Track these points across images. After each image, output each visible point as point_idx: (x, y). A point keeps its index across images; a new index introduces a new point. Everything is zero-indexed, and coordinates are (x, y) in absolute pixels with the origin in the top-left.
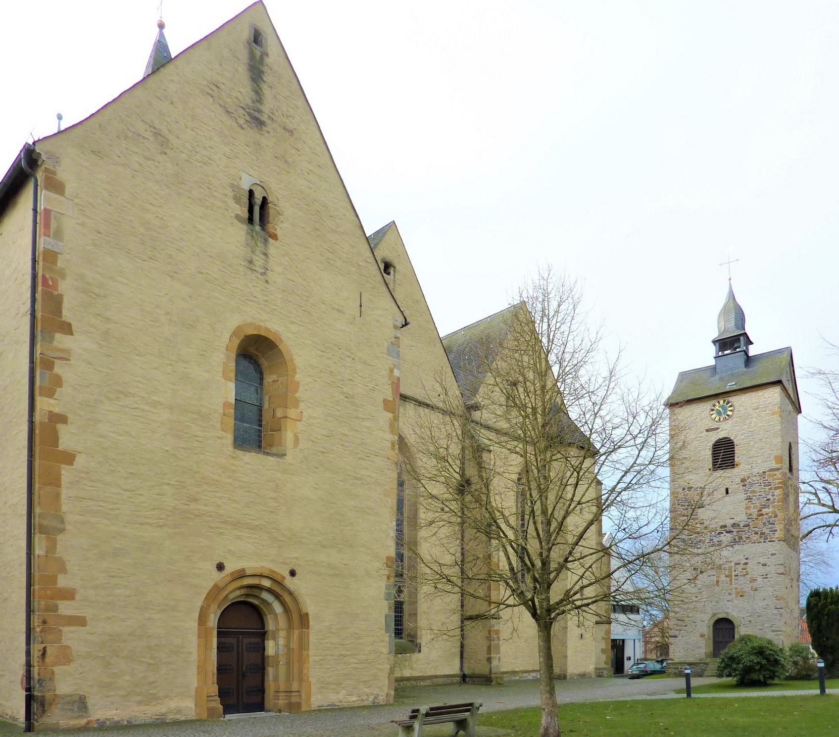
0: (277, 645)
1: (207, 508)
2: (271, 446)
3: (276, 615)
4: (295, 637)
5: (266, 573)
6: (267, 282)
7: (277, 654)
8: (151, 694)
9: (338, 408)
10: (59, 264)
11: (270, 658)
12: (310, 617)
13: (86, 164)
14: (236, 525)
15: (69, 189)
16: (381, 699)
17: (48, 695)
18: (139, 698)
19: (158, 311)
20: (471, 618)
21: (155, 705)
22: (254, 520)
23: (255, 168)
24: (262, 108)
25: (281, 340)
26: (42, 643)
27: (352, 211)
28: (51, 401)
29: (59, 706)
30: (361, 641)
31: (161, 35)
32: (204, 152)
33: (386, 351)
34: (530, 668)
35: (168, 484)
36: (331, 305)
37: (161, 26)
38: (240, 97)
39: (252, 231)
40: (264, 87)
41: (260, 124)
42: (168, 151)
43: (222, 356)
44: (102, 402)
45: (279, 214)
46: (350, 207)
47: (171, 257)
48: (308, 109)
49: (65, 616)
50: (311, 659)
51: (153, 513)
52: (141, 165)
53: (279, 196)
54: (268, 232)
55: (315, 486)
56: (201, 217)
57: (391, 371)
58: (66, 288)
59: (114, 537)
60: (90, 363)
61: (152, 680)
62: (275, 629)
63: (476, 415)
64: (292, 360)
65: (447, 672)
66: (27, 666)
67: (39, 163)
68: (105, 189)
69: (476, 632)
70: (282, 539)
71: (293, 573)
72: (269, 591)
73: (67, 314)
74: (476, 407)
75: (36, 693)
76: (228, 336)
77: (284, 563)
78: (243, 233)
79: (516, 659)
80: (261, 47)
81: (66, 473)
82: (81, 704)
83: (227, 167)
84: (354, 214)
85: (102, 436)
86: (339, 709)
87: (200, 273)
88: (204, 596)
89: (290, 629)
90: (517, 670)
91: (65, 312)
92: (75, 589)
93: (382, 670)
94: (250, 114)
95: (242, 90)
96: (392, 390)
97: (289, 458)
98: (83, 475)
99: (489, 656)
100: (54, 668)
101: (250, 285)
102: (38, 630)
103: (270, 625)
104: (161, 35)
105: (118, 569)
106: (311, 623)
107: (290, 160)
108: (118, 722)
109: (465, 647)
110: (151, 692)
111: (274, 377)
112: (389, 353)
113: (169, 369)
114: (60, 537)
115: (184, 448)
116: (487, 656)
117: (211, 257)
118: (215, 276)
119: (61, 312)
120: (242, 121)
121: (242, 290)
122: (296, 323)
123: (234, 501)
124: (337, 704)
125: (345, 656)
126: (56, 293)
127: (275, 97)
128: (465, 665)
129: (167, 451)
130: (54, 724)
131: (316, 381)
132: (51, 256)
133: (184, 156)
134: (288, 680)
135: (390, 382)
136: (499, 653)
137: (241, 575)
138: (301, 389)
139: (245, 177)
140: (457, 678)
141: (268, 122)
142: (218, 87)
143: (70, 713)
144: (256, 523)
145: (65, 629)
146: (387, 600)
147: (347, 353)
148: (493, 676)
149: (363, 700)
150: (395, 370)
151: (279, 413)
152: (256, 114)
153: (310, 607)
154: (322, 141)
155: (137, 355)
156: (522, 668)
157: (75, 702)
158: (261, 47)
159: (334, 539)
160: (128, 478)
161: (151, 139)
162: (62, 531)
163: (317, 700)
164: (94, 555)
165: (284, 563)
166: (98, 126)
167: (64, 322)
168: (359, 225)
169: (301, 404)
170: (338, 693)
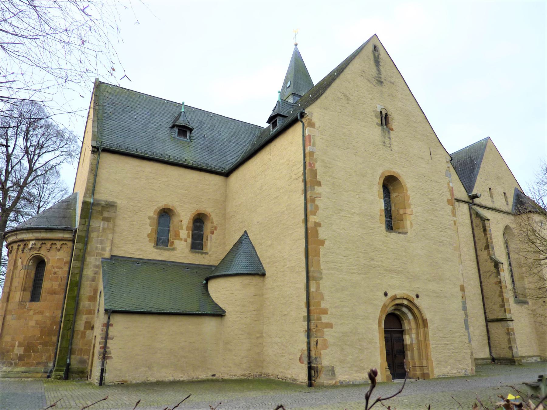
0: (411, 338)
1: (378, 263)
2: (398, 229)
3: (409, 320)
4: (421, 333)
5: (405, 297)
6: (392, 150)
7: (412, 344)
8: (361, 366)
9: (428, 206)
10: (315, 157)
11: (408, 347)
12: (428, 321)
13: (322, 114)
14: (390, 271)
15: (317, 125)
16: (469, 372)
17: (319, 366)
18: (356, 369)
19: (351, 171)
20: (493, 321)
21: (363, 373)
22: (397, 268)
23: (382, 101)
24: (381, 76)
25: (400, 176)
26: (316, 337)
27: (421, 112)
28: (315, 217)
29: (324, 373)
30: (454, 335)
31: (296, 48)
32: (362, 99)
33: (444, 175)
34: (531, 354)
35: (361, 252)
36: (418, 156)
37: (296, 45)
38: (373, 74)
39: (383, 129)
40: (381, 67)
41: (381, 83)
42: (349, 102)
43: (377, 187)
44: (333, 215)
45: (393, 119)
46: (420, 110)
47: (354, 146)
48: (398, 72)
49: (324, 323)
50: (431, 346)
51: (356, 267)
52: (341, 110)
53: (392, 111)
54: (389, 128)
55: (422, 248)
56: (364, 127)
57: (449, 184)
58: (318, 166)
59: (342, 281)
60: (328, 198)
61: (361, 359)
62: (408, 329)
63: (476, 201)
64: (405, 185)
65: (483, 356)
66: (308, 350)
67: (305, 117)
68: (329, 122)
69: (497, 329)
70: (411, 277)
71: (417, 296)
72: (407, 307)
73: (319, 178)
74: (476, 196)
75: (312, 365)
76: (379, 178)
77: (413, 291)
78: (380, 130)
79: (522, 348)
80: (377, 52)
81: (322, 250)
82: (332, 371)
83: (371, 103)
84: (422, 113)
85: (334, 231)
86: (448, 378)
87: (366, 151)
88: (380, 310)
89: (418, 328)
90: (524, 355)
91: (318, 177)
92: (328, 308)
93: (467, 353)
94: (377, 80)
95: (373, 71)
96: (450, 194)
97: (409, 234)
98: (328, 251)
99: (510, 345)
100: (321, 351)
101: (385, 153)
102: (314, 331)
103: (406, 326)
104: (296, 48)
105: (344, 297)
106: (429, 324)
107: (394, 95)
108: (348, 382)
109: (491, 339)
110: (361, 365)
111: (397, 194)
112: (446, 176)
113: (357, 197)
114: (321, 282)
115: (366, 234)
116: (508, 346)
117: (369, 143)
118: (371, 151)
119: (317, 177)
120: (374, 84)
121: (382, 156)
122: (405, 167)
123: (388, 259)
124: (447, 375)
125: (447, 345)
126: (314, 169)
127: (385, 71)
128: (493, 351)
129: (359, 236)
130: (322, 383)
131: (416, 194)
132: (312, 153)
133: (355, 103)
134: (420, 359)
135: (449, 190)
136: (516, 344)
137: (395, 298)
138: (411, 198)
139: (378, 106)
140: (489, 360)
141: (384, 81)
142: (364, 72)
143: (328, 377)
144: (399, 269)
145: (325, 330)
146: (464, 310)
147: (428, 178)
148: (515, 359)
149: (459, 373)
150: (450, 184)
151: (401, 212)
152: (379, 79)
153: (428, 315)
154: (405, 84)
155: (345, 192)
156: (526, 354)
157: (330, 370)
158: (377, 52)
159: (434, 276)
160: (345, 250)
161: (343, 98)
162: (321, 278)
163: (437, 371)
164: (334, 290)
165: (413, 291)
166: (325, 98)
167: (318, 181)
168: (425, 117)
169: (412, 206)
170: (446, 367)
